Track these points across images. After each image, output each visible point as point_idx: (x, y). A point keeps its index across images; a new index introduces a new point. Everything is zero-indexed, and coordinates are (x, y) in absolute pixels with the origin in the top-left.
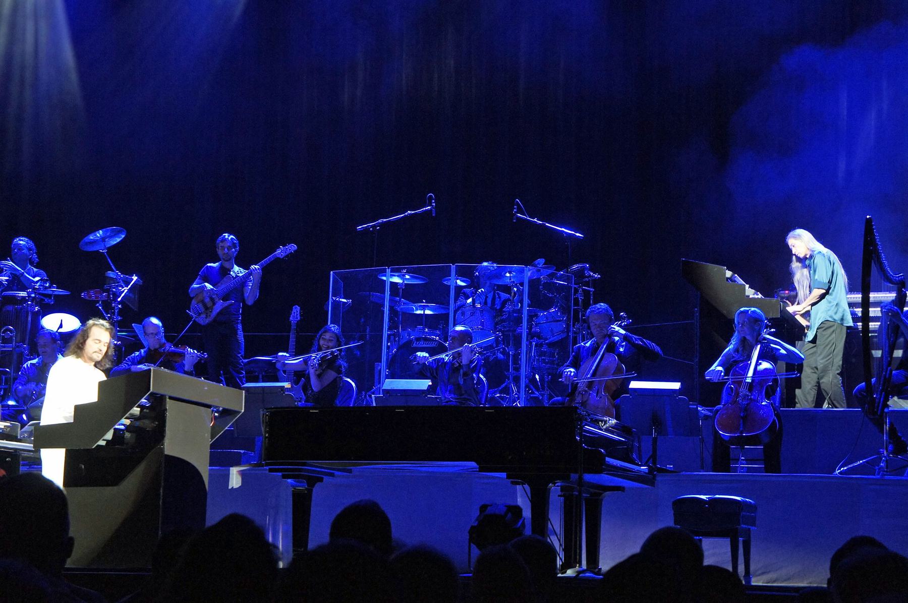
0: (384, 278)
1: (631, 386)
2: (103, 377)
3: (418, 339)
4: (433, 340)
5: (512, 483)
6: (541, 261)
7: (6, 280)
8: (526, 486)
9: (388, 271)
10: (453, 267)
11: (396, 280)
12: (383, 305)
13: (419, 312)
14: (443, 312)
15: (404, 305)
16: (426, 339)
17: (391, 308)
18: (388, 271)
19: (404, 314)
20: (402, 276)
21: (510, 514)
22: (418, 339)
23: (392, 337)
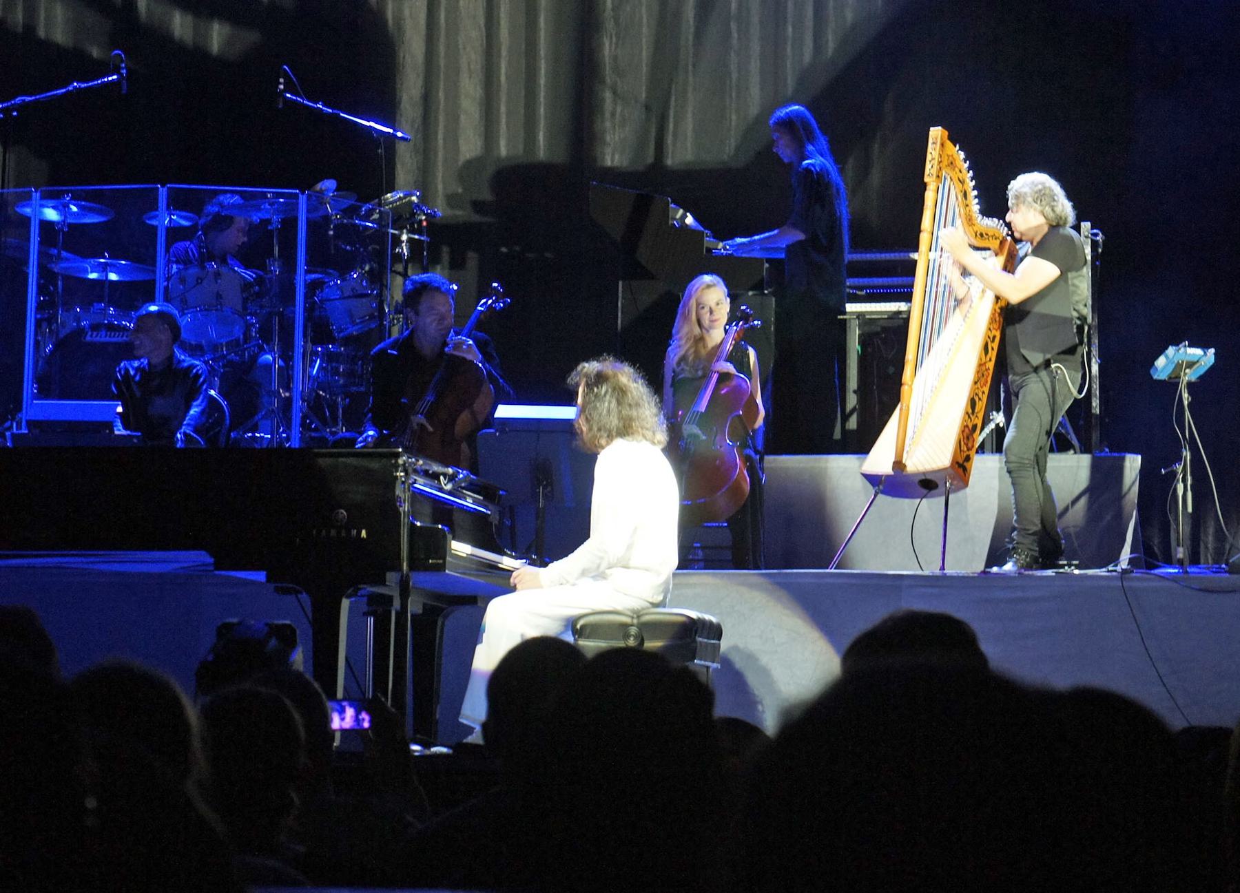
0: (28, 210)
1: (496, 415)
2: (420, 611)
3: (95, 327)
4: (125, 328)
5: (277, 590)
6: (329, 185)
7: (716, 670)
8: (305, 598)
9: (36, 196)
10: (163, 192)
11: (51, 214)
12: (26, 262)
13: (93, 276)
14: (139, 277)
15: (66, 263)
16: (110, 328)
17: (41, 267)
18: (36, 196)
19: (66, 278)
20: (62, 208)
21: (273, 642)
22: (95, 327)
23: (44, 324)
